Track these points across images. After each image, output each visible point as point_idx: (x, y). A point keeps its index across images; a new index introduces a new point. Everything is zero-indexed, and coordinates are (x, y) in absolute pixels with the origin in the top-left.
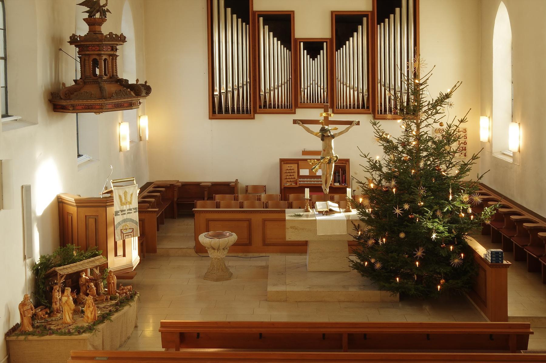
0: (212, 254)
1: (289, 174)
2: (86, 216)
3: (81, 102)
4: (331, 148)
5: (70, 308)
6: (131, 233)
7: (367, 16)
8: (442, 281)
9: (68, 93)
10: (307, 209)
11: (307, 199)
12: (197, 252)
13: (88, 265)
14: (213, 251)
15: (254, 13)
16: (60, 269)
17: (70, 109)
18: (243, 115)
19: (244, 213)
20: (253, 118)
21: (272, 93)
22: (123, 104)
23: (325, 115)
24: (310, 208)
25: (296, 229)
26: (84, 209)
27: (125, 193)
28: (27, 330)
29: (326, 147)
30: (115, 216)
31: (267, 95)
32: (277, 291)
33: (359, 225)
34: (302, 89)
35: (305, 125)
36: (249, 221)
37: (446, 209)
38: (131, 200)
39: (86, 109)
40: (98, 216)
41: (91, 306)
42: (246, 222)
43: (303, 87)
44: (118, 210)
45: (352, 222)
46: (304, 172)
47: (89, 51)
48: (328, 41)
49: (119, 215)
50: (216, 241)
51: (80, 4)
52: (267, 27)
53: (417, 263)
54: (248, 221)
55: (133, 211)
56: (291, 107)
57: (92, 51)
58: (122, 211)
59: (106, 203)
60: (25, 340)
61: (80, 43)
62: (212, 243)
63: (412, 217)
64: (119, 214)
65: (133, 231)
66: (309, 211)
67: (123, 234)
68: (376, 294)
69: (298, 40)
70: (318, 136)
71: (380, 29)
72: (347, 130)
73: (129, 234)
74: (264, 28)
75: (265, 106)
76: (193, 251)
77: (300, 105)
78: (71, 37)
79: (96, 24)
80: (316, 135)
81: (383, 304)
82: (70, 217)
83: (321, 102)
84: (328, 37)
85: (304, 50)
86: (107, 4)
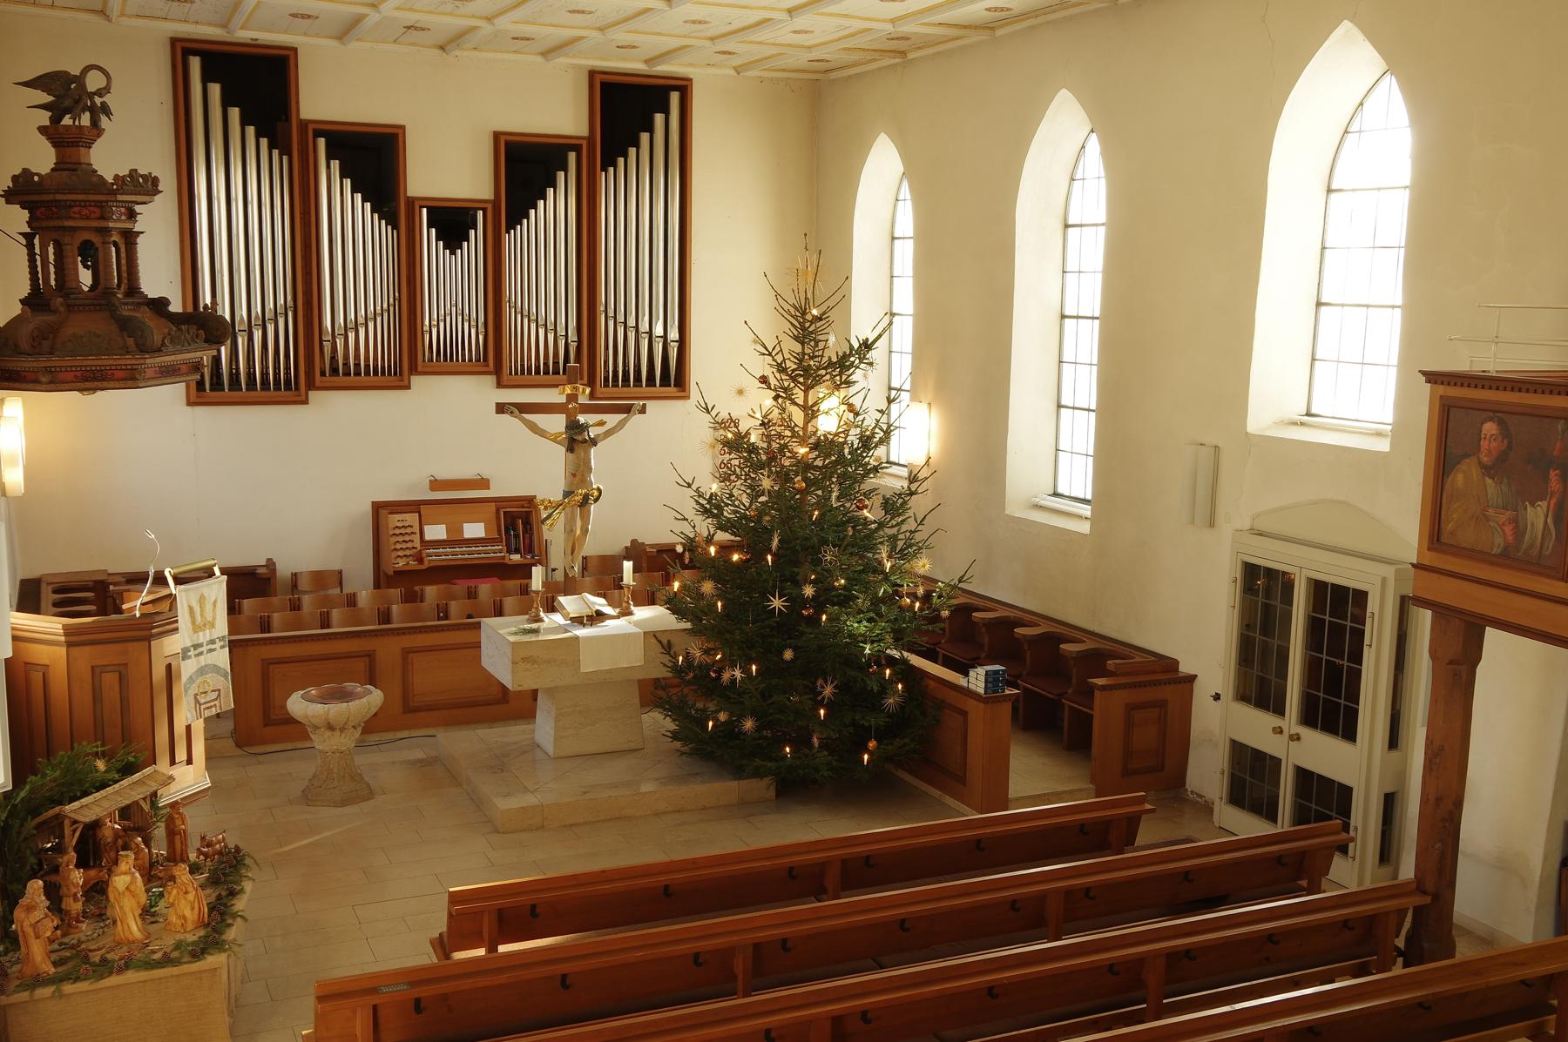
0: (323, 742)
1: (400, 539)
2: (93, 668)
3: (68, 361)
4: (590, 469)
5: (138, 903)
6: (216, 702)
7: (577, 148)
8: (872, 744)
9: (37, 336)
10: (628, 608)
11: (537, 592)
12: (238, 745)
13: (133, 793)
14: (328, 733)
15: (304, 125)
16: (75, 808)
17: (44, 379)
18: (278, 393)
19: (365, 636)
20: (305, 402)
21: (351, 336)
22: (177, 366)
23: (569, 392)
24: (544, 612)
25: (534, 662)
26: (87, 649)
27: (202, 599)
28: (45, 972)
29: (578, 468)
30: (183, 660)
31: (340, 342)
32: (522, 808)
33: (669, 642)
34: (426, 328)
35: (527, 416)
36: (370, 656)
37: (882, 590)
38: (214, 619)
39: (87, 381)
40: (126, 664)
41: (190, 889)
42: (363, 659)
43: (427, 322)
44: (188, 644)
45: (655, 636)
46: (436, 532)
47: (73, 218)
48: (489, 207)
49: (190, 656)
50: (336, 710)
51: (27, 84)
52: (335, 164)
53: (822, 712)
54: (369, 656)
55: (218, 644)
56: (398, 373)
57: (81, 219)
58: (196, 646)
59: (151, 630)
60: (59, 995)
61: (52, 196)
62: (331, 715)
63: (809, 614)
64: (189, 654)
65: (219, 695)
66: (541, 620)
67: (200, 705)
68: (727, 789)
69: (416, 202)
70: (559, 443)
71: (605, 180)
72: (621, 425)
73: (212, 704)
74: (328, 167)
75: (335, 371)
76: (230, 743)
77: (423, 367)
78: (15, 178)
79: (66, 144)
80: (554, 441)
81: (745, 809)
82: (37, 677)
83: (470, 360)
84: (487, 198)
85: (429, 227)
86: (110, 89)
